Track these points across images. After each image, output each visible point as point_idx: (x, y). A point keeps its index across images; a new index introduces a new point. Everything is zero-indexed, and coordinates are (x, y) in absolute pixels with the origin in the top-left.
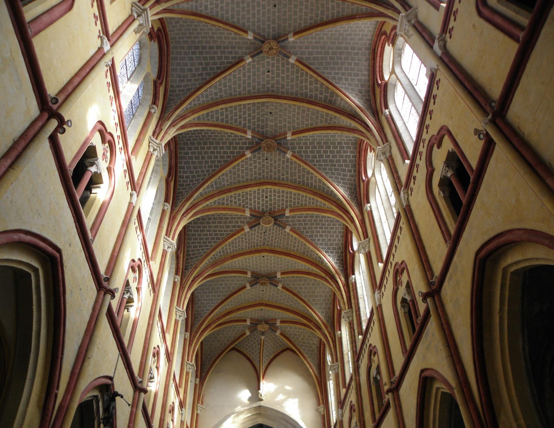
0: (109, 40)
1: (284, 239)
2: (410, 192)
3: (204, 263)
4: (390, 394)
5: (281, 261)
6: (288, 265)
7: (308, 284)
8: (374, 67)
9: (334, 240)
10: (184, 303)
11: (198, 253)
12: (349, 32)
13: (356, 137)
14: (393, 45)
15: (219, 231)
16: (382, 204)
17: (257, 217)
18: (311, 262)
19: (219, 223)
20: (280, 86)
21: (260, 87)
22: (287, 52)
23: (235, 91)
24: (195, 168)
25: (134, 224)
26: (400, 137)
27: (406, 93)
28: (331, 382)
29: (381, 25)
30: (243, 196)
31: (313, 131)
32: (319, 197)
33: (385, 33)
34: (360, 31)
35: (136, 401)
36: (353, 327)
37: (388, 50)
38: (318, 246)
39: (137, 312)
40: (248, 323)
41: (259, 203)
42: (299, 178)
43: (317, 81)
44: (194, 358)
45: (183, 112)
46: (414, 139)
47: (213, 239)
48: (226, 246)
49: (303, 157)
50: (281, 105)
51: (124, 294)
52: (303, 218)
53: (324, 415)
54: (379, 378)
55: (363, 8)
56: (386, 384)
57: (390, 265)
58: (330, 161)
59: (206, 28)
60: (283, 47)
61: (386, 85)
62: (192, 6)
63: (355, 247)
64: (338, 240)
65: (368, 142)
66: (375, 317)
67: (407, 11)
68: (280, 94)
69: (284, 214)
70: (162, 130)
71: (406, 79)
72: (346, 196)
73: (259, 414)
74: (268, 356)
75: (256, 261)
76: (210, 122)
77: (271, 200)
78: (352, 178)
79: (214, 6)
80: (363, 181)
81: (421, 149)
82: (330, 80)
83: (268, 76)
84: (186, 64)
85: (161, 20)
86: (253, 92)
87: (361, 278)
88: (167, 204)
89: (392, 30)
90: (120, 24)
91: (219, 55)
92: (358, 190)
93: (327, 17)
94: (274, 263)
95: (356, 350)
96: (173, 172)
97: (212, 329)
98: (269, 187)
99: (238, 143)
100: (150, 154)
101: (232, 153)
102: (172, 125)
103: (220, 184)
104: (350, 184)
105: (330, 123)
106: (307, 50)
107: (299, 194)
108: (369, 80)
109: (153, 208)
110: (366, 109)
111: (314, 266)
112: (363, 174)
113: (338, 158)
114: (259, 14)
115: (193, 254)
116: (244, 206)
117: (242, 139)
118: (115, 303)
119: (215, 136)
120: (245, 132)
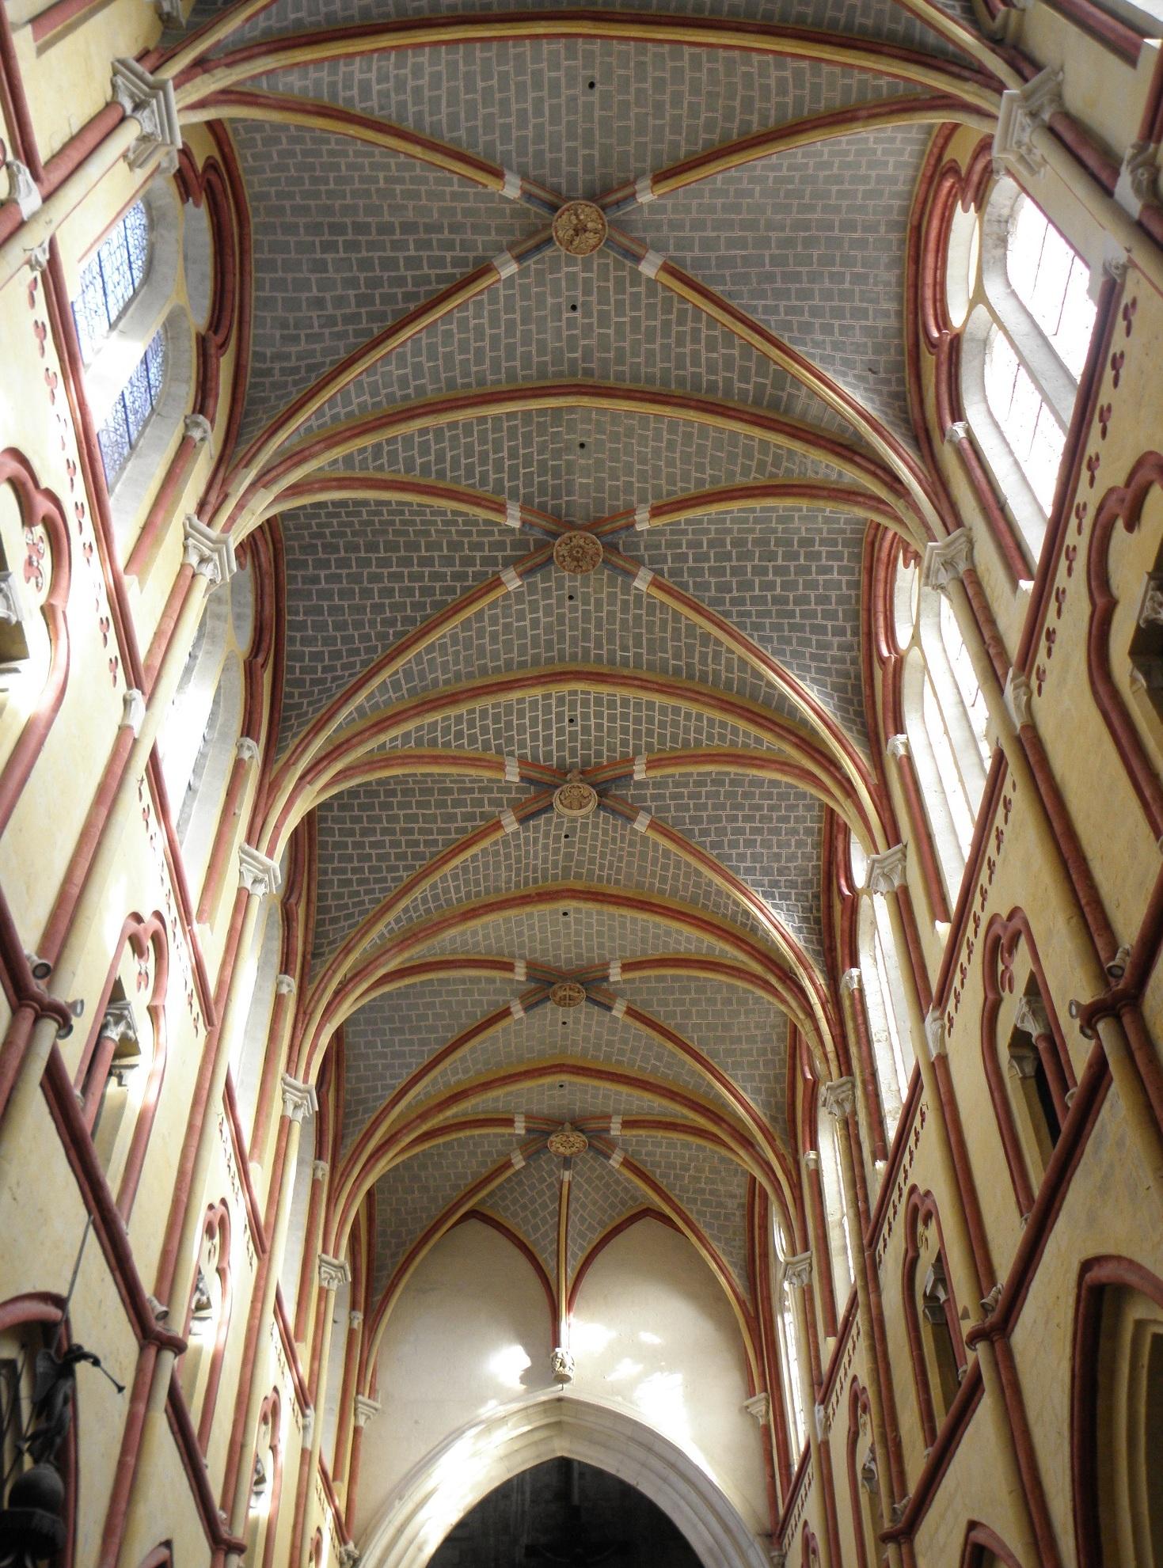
0: (36, 177)
1: (631, 854)
2: (1034, 683)
3: (374, 934)
4: (981, 1346)
5: (623, 926)
6: (644, 941)
7: (711, 1001)
8: (916, 286)
9: (792, 857)
10: (308, 1064)
11: (355, 905)
12: (835, 171)
13: (858, 521)
14: (979, 208)
15: (421, 831)
16: (946, 732)
17: (543, 787)
18: (719, 928)
19: (420, 805)
20: (612, 355)
21: (548, 358)
22: (633, 240)
23: (466, 374)
24: (340, 626)
25: (135, 800)
26: (1002, 508)
27: (1023, 362)
28: (789, 1317)
29: (940, 141)
30: (496, 719)
31: (721, 500)
32: (741, 716)
33: (953, 169)
34: (870, 166)
35: (148, 1380)
36: (857, 1136)
37: (965, 223)
38: (739, 878)
39: (152, 1086)
40: (520, 1128)
41: (548, 740)
42: (677, 656)
43: (729, 335)
44: (345, 1242)
45: (295, 439)
46: (1049, 511)
47: (402, 857)
48: (444, 879)
49: (687, 590)
50: (615, 417)
51: (104, 1027)
52: (692, 789)
53: (767, 1428)
54: (942, 1296)
55: (883, 82)
56: (966, 1315)
57: (971, 925)
58: (776, 600)
59: (366, 161)
60: (620, 226)
61: (956, 342)
62: (318, 83)
63: (860, 878)
64: (803, 855)
65: (902, 532)
66: (927, 1098)
67: (1026, 80)
68: (611, 382)
69: (630, 775)
70: (226, 496)
71: (1023, 318)
72: (828, 711)
73: (558, 1425)
74: (582, 1235)
75: (542, 930)
76: (386, 475)
77: (586, 730)
78: (848, 655)
79: (391, 84)
80: (883, 662)
81: (1071, 538)
82: (774, 333)
83: (571, 323)
84: (304, 285)
85: (212, 126)
86: (524, 377)
87: (878, 973)
88: (249, 742)
89: (975, 158)
90: (75, 130)
91: (412, 253)
92: (865, 690)
93: (764, 118)
94: (600, 934)
95: (867, 1210)
96: (270, 638)
97: (403, 1151)
98: (579, 686)
99: (478, 546)
100: (189, 573)
101: (459, 577)
102: (262, 481)
103: (422, 678)
104: (839, 674)
105: (773, 476)
106: (697, 235)
107: (676, 711)
108: (900, 330)
109: (202, 755)
110: (891, 423)
111: (727, 940)
112: (882, 638)
113: (800, 591)
114: (538, 112)
115: (339, 908)
116: (499, 751)
117: (492, 533)
118: (73, 1053)
119: (404, 523)
120: (501, 509)
